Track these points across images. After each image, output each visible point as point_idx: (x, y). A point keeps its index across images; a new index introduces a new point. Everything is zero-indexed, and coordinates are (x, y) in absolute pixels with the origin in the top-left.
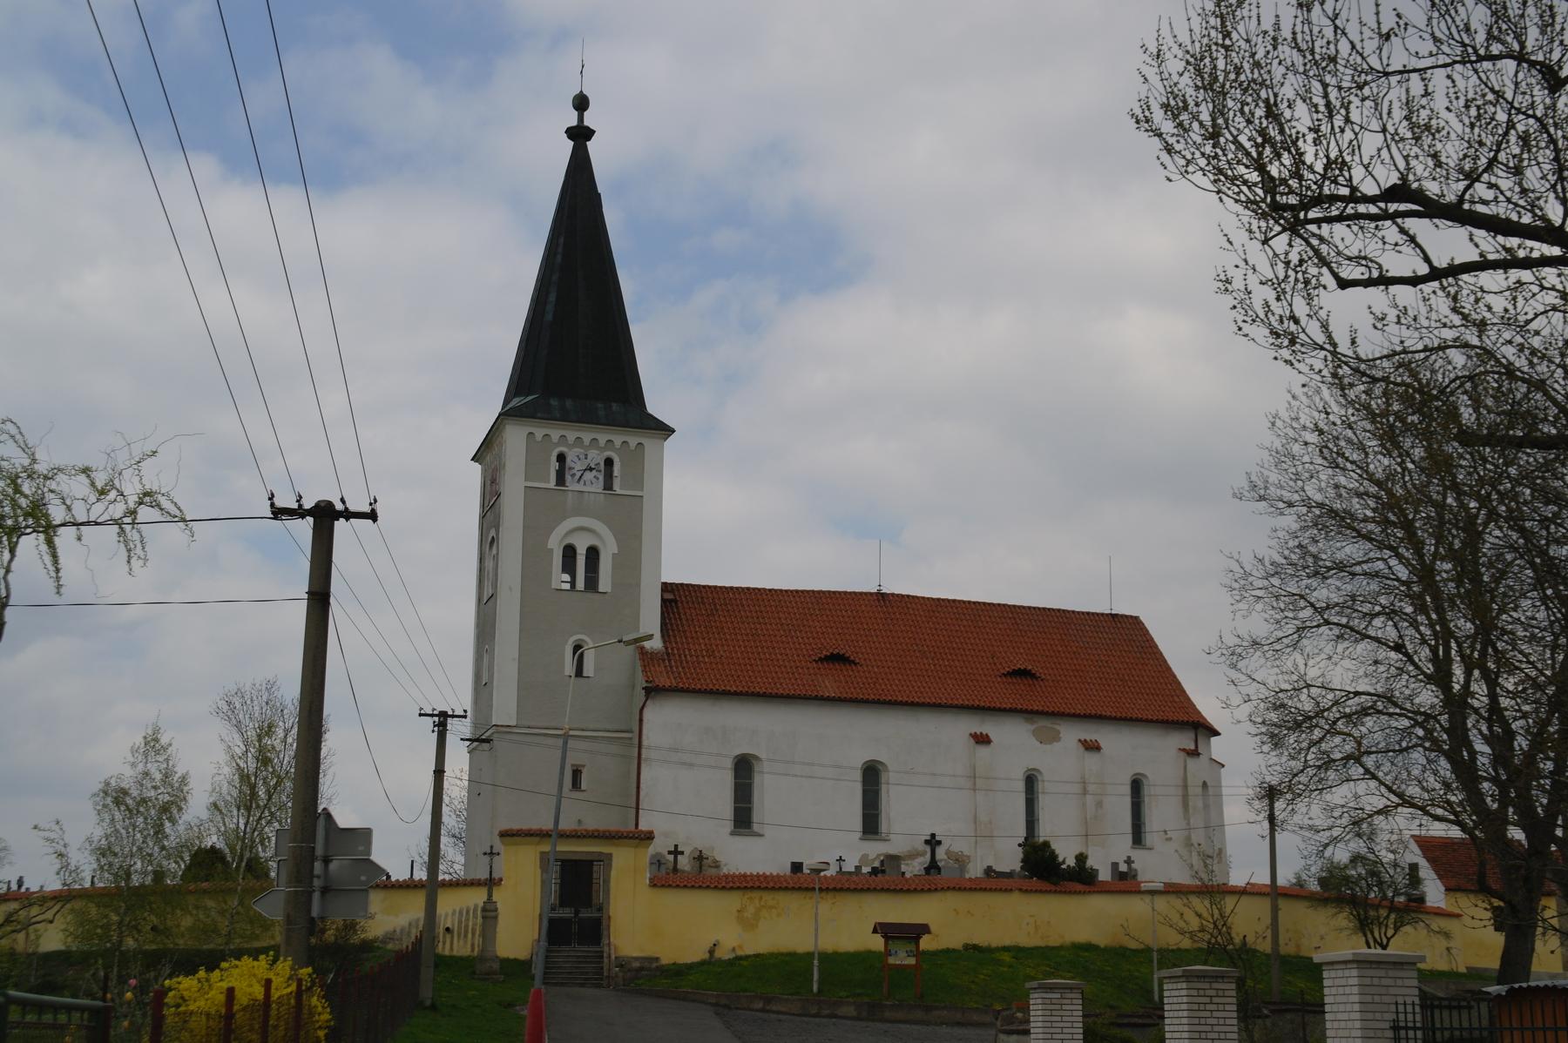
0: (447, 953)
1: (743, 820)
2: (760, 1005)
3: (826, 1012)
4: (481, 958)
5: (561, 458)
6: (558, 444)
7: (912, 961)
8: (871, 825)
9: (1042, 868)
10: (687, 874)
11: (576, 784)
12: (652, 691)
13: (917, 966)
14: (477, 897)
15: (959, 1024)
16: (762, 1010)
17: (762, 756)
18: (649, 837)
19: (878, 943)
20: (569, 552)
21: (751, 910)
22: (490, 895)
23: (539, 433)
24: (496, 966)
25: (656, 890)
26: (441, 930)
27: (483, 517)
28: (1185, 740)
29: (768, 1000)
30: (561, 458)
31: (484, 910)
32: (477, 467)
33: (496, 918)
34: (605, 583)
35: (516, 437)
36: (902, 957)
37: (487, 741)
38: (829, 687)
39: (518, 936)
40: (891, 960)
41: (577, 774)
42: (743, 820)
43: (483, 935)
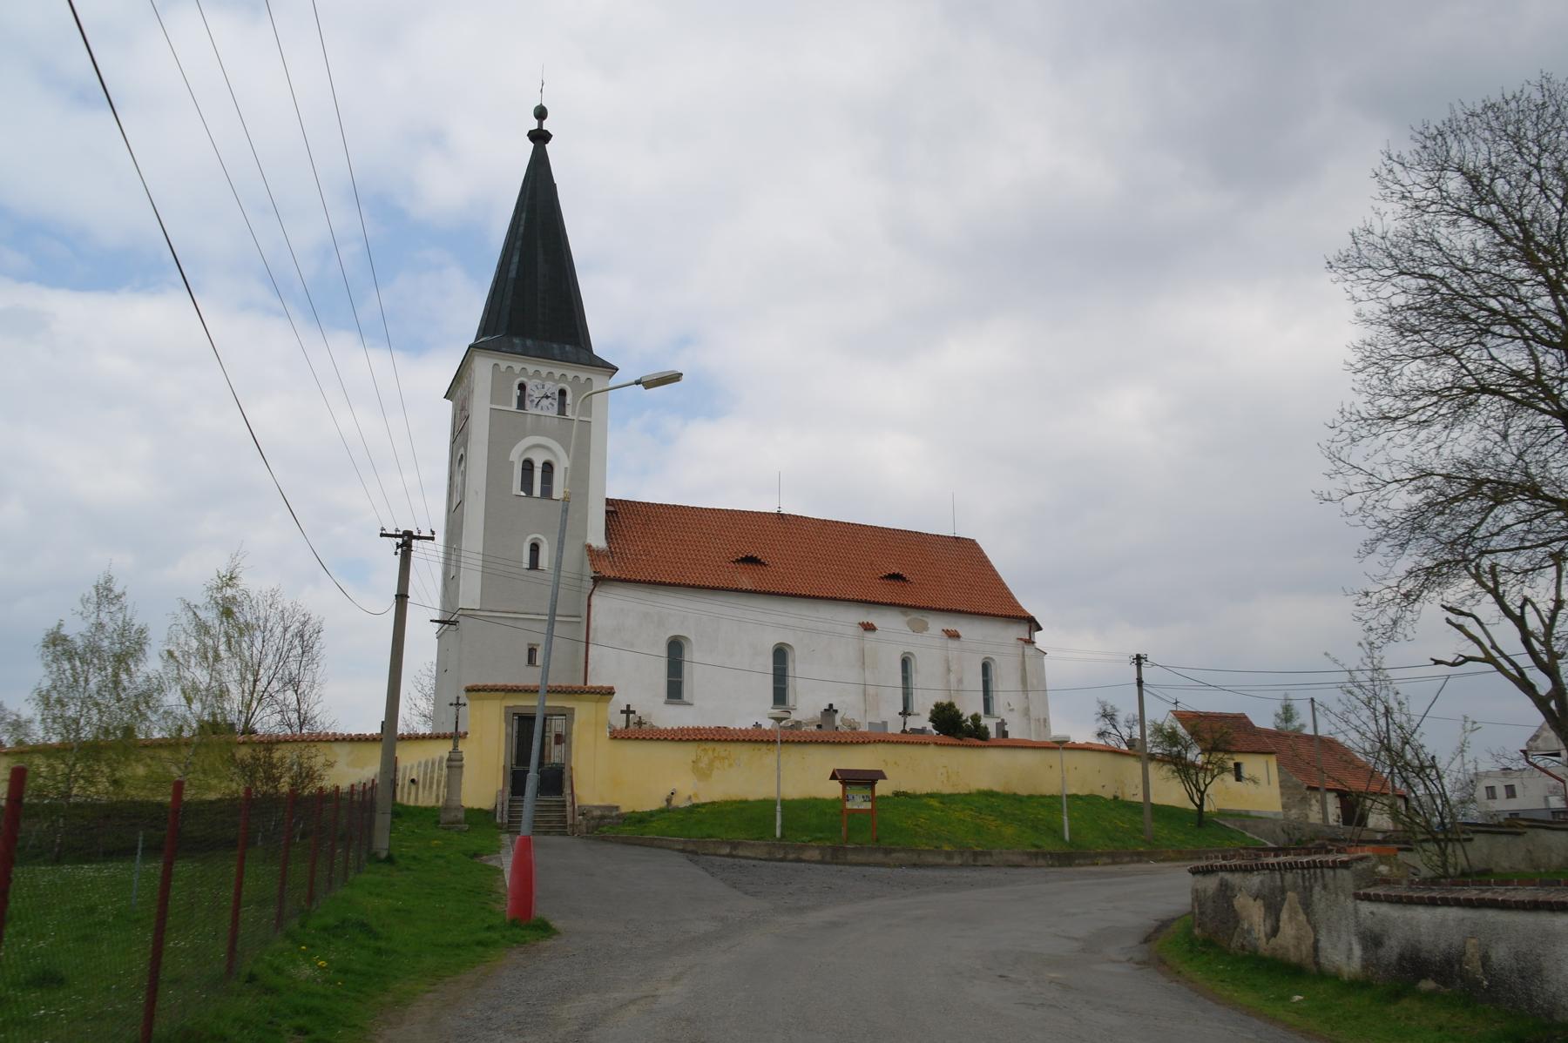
0: (412, 803)
1: (675, 691)
2: (727, 850)
3: (791, 856)
4: (446, 808)
5: (522, 387)
6: (519, 376)
7: (868, 806)
8: (780, 696)
9: (949, 723)
10: (635, 731)
11: (532, 652)
12: (599, 580)
13: (872, 811)
14: (443, 750)
15: (915, 866)
16: (729, 856)
17: (692, 638)
18: (610, 692)
19: (834, 790)
20: (528, 466)
21: (705, 760)
22: (456, 747)
23: (503, 365)
24: (461, 815)
25: (616, 743)
26: (407, 782)
27: (453, 442)
28: (1021, 631)
29: (735, 846)
30: (522, 387)
31: (449, 760)
32: (450, 403)
33: (461, 767)
34: (558, 492)
35: (484, 367)
36: (859, 802)
37: (455, 623)
38: (746, 583)
39: (482, 785)
40: (849, 806)
41: (531, 660)
42: (675, 691)
43: (448, 785)
